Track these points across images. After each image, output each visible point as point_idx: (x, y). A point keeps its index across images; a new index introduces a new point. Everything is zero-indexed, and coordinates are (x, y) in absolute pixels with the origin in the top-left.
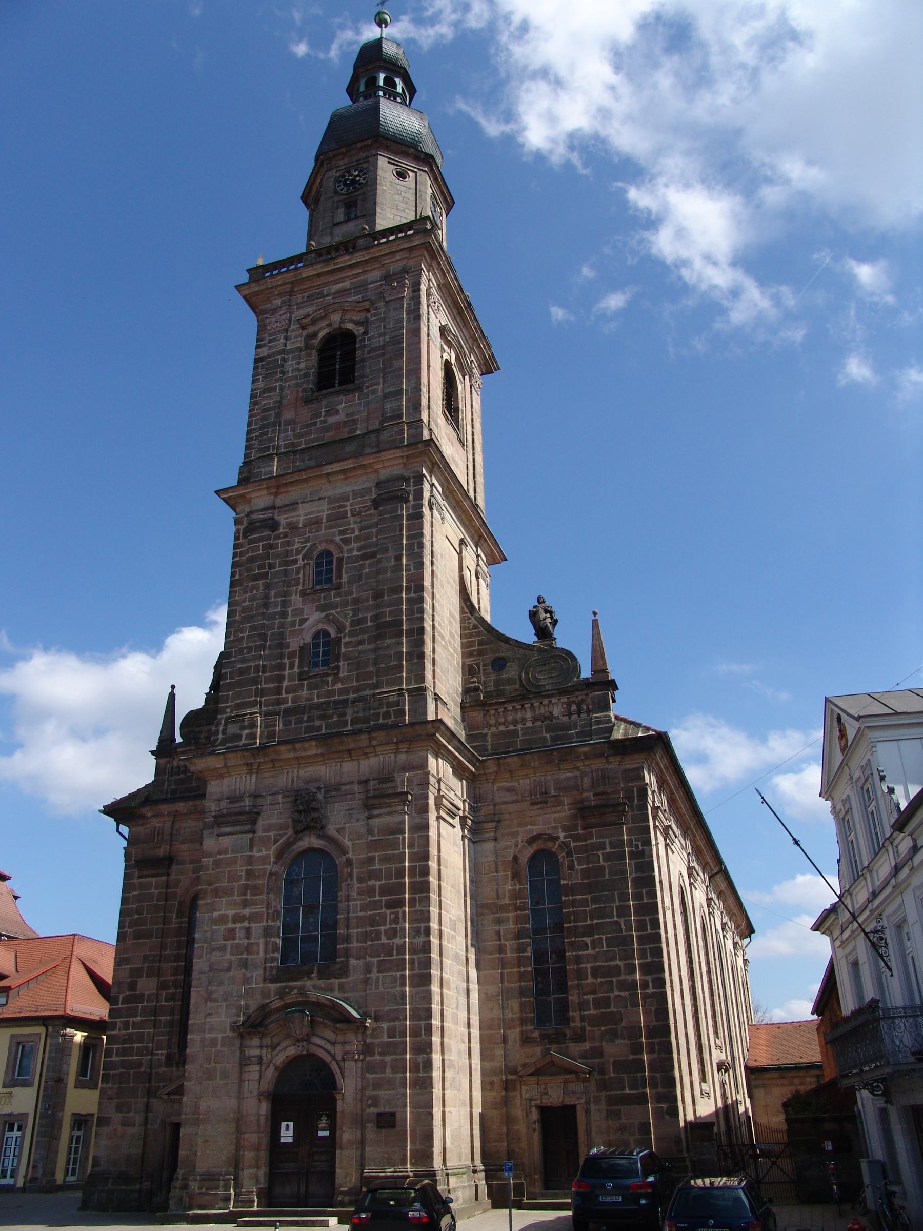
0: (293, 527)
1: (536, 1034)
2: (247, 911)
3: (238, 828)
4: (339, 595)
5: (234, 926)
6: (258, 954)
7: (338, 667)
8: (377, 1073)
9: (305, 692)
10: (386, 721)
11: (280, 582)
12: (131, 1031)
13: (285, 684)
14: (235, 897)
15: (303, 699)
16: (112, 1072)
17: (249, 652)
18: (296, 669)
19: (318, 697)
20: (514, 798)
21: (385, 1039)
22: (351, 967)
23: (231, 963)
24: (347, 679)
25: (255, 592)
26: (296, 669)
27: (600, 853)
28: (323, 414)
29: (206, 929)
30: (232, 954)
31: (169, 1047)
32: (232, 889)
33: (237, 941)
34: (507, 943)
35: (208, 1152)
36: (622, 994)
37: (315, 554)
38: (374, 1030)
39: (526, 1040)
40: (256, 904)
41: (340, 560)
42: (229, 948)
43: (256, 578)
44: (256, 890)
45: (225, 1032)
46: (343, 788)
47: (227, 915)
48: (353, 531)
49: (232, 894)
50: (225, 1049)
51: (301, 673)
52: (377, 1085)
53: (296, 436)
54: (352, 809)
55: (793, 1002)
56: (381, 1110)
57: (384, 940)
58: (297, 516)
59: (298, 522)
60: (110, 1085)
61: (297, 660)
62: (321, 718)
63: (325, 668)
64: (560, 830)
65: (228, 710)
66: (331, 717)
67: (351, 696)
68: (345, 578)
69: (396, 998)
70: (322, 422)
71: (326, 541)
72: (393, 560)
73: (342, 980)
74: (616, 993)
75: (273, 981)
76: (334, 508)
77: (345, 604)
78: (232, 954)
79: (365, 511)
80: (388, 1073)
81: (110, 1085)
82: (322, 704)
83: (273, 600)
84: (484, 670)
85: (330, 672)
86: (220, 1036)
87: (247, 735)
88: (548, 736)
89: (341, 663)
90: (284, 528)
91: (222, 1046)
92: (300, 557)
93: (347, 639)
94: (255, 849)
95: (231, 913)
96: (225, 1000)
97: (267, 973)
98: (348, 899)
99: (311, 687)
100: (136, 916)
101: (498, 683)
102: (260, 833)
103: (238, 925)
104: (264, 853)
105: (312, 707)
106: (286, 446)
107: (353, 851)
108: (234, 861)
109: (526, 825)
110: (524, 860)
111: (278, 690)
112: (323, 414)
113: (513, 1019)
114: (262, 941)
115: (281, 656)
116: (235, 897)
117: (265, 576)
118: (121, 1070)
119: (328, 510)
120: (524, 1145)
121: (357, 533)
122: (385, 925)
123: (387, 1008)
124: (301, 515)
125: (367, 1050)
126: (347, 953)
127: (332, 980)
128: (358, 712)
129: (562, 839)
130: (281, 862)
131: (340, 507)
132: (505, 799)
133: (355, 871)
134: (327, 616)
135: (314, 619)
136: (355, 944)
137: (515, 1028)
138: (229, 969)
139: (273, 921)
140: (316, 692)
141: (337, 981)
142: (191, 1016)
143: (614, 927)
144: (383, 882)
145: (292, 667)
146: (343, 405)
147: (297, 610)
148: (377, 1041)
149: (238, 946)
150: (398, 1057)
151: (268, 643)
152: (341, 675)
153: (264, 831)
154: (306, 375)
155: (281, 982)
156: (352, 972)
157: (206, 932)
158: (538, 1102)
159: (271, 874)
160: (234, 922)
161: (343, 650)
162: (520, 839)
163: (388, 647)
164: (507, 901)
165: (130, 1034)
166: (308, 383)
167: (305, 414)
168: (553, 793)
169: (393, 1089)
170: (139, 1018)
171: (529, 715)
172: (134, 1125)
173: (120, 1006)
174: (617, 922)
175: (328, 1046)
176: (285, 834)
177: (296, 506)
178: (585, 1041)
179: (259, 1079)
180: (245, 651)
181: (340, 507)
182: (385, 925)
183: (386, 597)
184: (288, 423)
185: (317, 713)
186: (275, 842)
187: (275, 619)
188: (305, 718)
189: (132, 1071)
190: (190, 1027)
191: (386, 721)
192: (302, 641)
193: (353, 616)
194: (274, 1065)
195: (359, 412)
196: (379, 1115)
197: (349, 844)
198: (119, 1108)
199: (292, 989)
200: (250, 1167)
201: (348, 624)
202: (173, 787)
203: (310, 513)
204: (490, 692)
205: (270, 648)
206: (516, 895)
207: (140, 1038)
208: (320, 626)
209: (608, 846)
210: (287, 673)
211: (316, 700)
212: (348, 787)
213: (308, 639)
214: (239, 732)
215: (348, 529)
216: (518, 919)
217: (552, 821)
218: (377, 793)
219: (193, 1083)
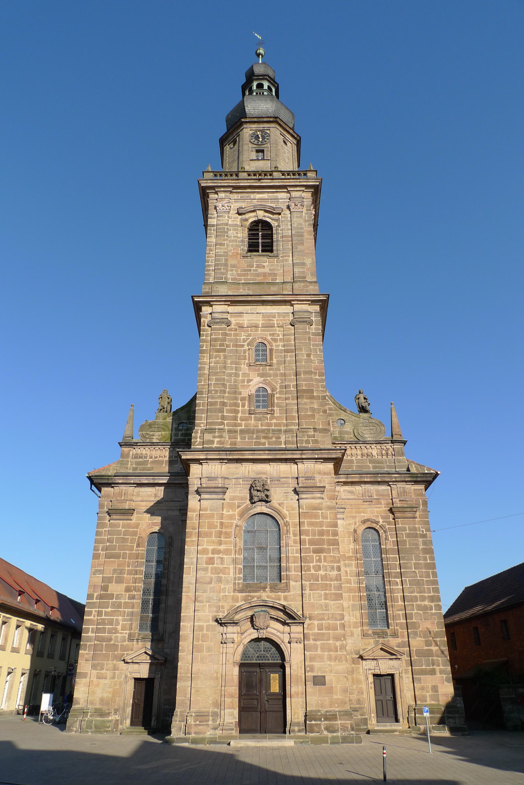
0: (241, 327)
1: (370, 632)
2: (222, 547)
3: (214, 496)
4: (272, 369)
5: (213, 556)
6: (229, 574)
8: (312, 651)
9: (253, 421)
10: (307, 445)
11: (233, 356)
12: (103, 617)
13: (240, 415)
14: (213, 538)
15: (252, 426)
16: (88, 643)
17: (215, 393)
18: (246, 407)
19: (262, 425)
21: (316, 631)
22: (291, 586)
23: (211, 579)
24: (277, 418)
25: (218, 359)
26: (246, 407)
27: (404, 533)
28: (255, 266)
30: (212, 573)
31: (131, 629)
32: (211, 533)
33: (215, 565)
34: (352, 578)
35: (198, 698)
36: (419, 612)
39: (364, 635)
40: (227, 544)
41: (271, 350)
42: (210, 569)
43: (218, 351)
45: (208, 621)
46: (282, 480)
47: (208, 549)
48: (278, 335)
49: (211, 536)
50: (209, 633)
51: (250, 410)
52: (312, 659)
53: (239, 275)
55: (59, 621)
56: (316, 674)
57: (313, 572)
58: (243, 320)
59: (244, 324)
60: (87, 652)
61: (247, 402)
62: (265, 438)
63: (265, 409)
64: (380, 518)
65: (202, 425)
66: (271, 438)
67: (283, 428)
68: (275, 361)
70: (254, 270)
71: (262, 338)
72: (305, 356)
73: (286, 594)
74: (416, 611)
75: (241, 591)
76: (267, 320)
77: (276, 375)
78: (212, 573)
79: (285, 326)
80: (319, 652)
81: (87, 652)
82: (264, 430)
83: (229, 365)
84: (333, 424)
85: (268, 412)
86: (205, 624)
88: (371, 465)
89: (275, 408)
90: (234, 325)
91: (207, 631)
92: (246, 343)
93: (278, 395)
94: (225, 510)
95: (210, 548)
96: (209, 602)
98: (287, 545)
99: (256, 419)
100: (108, 544)
101: (340, 433)
102: (228, 500)
105: (258, 431)
106: (232, 279)
107: (289, 517)
108: (212, 516)
109: (360, 513)
110: (360, 531)
111: (235, 418)
112: (255, 266)
113: (356, 623)
114: (232, 567)
115: (236, 399)
116: (213, 538)
117: (224, 351)
118: (96, 642)
119: (262, 320)
120: (365, 696)
121: (281, 337)
122: (313, 562)
123: (316, 612)
124: (245, 320)
125: (305, 636)
126: (288, 578)
127: (280, 593)
128: (288, 438)
129: (381, 523)
133: (291, 529)
134: (264, 380)
135: (256, 382)
136: (293, 573)
137: (357, 627)
138: (210, 583)
139: (239, 555)
140: (260, 422)
141: (283, 594)
142: (182, 611)
143: (413, 575)
144: (310, 537)
145: (243, 406)
146: (267, 263)
147: (245, 373)
149: (216, 568)
150: (326, 642)
151: (227, 390)
152: (275, 415)
154: (242, 241)
155: (246, 592)
156: (292, 589)
158: (373, 671)
159: (237, 526)
160: (213, 553)
161: (276, 401)
162: (357, 520)
163: (305, 404)
165: (104, 620)
166: (244, 246)
167: (244, 263)
168: (375, 497)
169: (322, 662)
170: (109, 609)
171: (359, 452)
172: (106, 678)
173: (95, 600)
174: (415, 571)
175: (278, 634)
177: (242, 314)
178: (398, 637)
179: (235, 653)
180: (213, 392)
182: (313, 562)
183: (302, 376)
184: (233, 266)
185: (262, 435)
186: (239, 507)
188: (255, 437)
189: (104, 643)
190: (182, 618)
191: (307, 445)
192: (250, 392)
193: (282, 383)
194: (243, 644)
196: (314, 677)
197: (287, 513)
198: (94, 667)
199: (253, 597)
200: (229, 708)
201: (278, 387)
202: (134, 466)
204: (336, 437)
205: (229, 393)
206: (356, 552)
207: (111, 622)
209: (407, 529)
210: (240, 409)
211: (260, 427)
212: (285, 479)
213: (253, 392)
214: (212, 439)
215: (276, 334)
216: (357, 566)
217: (378, 512)
219: (185, 654)
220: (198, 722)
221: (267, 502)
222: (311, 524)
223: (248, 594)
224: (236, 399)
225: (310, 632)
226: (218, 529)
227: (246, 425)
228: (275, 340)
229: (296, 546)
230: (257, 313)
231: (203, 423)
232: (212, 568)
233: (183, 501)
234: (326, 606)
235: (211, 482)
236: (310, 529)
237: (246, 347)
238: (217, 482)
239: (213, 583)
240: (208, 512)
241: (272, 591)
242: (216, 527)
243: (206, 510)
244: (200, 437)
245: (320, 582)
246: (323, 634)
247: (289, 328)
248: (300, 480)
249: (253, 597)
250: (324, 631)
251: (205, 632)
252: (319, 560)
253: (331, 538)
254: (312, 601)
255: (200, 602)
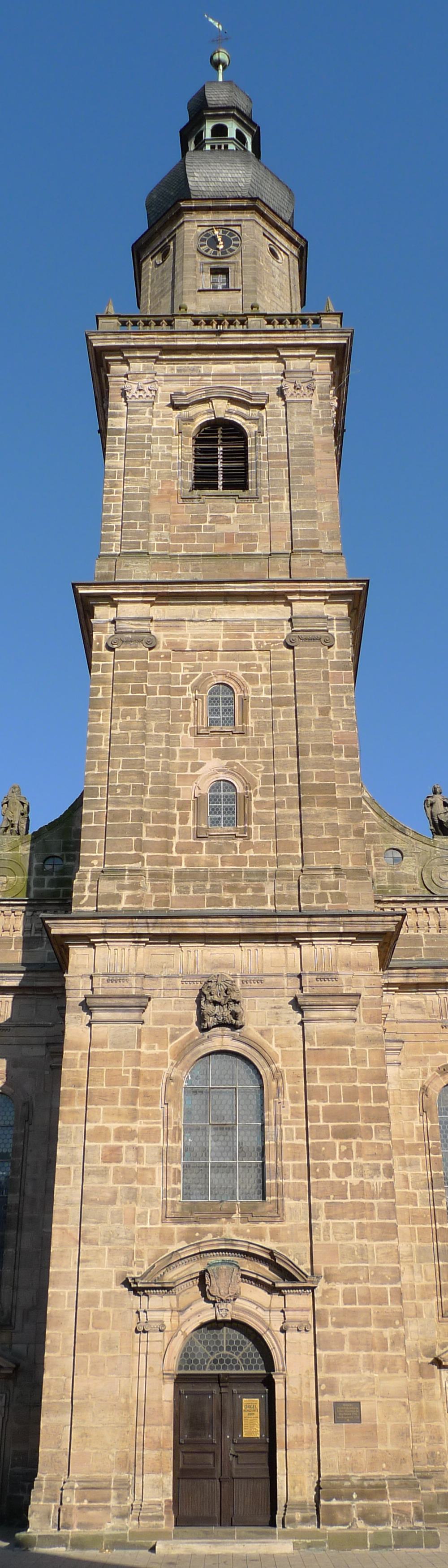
0: (179, 650)
3: (120, 1015)
4: (245, 742)
5: (118, 1144)
6: (153, 1183)
7: (247, 830)
8: (331, 1349)
9: (204, 854)
11: (162, 712)
13: (176, 840)
15: (202, 863)
17: (123, 793)
18: (190, 824)
19: (223, 863)
20: (420, 1017)
21: (341, 1305)
22: (286, 1209)
23: (115, 1193)
24: (256, 847)
25: (128, 719)
29: (73, 1145)
30: (116, 1181)
32: (114, 1095)
33: (123, 1164)
35: (87, 1450)
37: (209, 687)
38: (325, 1292)
40: (148, 1118)
41: (244, 700)
42: (111, 1173)
43: (130, 702)
44: (150, 1099)
46: (267, 980)
47: (107, 1129)
48: (259, 668)
50: (111, 1310)
51: (197, 830)
52: (332, 1366)
53: (174, 538)
54: (280, 1008)
56: (339, 1399)
57: (333, 1177)
58: (183, 636)
59: (185, 643)
61: (191, 812)
62: (230, 889)
65: (95, 862)
66: (244, 890)
67: (269, 868)
68: (251, 723)
69: (353, 1253)
71: (225, 674)
72: (317, 712)
75: (178, 1220)
76: (234, 636)
77: (254, 754)
78: (116, 1181)
82: (229, 873)
84: (376, 860)
86: (101, 1291)
87: (128, 897)
89: (252, 826)
90: (164, 647)
91: (105, 1305)
92: (189, 686)
93: (258, 798)
94: (144, 1045)
95: (113, 1126)
97: (169, 1210)
98: (278, 1121)
99: (211, 849)
102: (149, 1024)
103: (125, 1144)
104: (157, 1051)
105: (215, 875)
106: (159, 547)
107: (283, 1060)
108: (116, 1058)
111: (167, 847)
112: (209, 519)
114: (158, 1167)
115: (168, 805)
116: (119, 1106)
117: (142, 701)
121: (265, 671)
122: (334, 1158)
123: (341, 1265)
124: (188, 636)
127: (262, 1225)
128: (281, 889)
130: (181, 1066)
131: (241, 636)
132: (410, 1017)
133: (287, 1085)
134: (228, 765)
135: (212, 768)
136: (291, 1180)
138: (112, 1201)
140: (220, 856)
141: (268, 1226)
144: (328, 1103)
145: (184, 820)
146: (235, 513)
147: (188, 750)
148: (329, 1307)
149: (124, 1171)
150: (361, 1329)
151: (149, 786)
152: (252, 840)
153: (156, 1022)
154: (182, 466)
155: (189, 1222)
156: (288, 1216)
157: (73, 1148)
159: (170, 1079)
160: (118, 1138)
161: (254, 810)
162: (429, 1067)
163: (317, 816)
164: (415, 1141)
167: (185, 512)
169: (354, 1371)
175: (259, 1312)
176: (186, 1029)
177: (182, 623)
179: (165, 1353)
180: (119, 791)
181: (241, 636)
182: (334, 1158)
183: (310, 756)
184: (162, 519)
186: (174, 1037)
187: (159, 757)
188: (208, 887)
190: (51, 1278)
194: (184, 1333)
195: (258, 527)
196: (336, 1404)
197: (278, 1051)
199: (204, 1233)
200: (153, 1472)
201: (259, 779)
203: (200, 636)
204: (384, 887)
208: (222, 776)
210: (177, 826)
211: (220, 867)
212: (273, 979)
213: (205, 790)
214: (116, 892)
215: (253, 665)
218: (316, 991)
219: (58, 1354)
220: (86, 1503)
221: (234, 1027)
222: (330, 1075)
223: (193, 1226)
224: (168, 805)
225: (329, 1307)
226: (130, 1086)
227: (189, 862)
228: (253, 679)
229: (297, 1123)
230: (214, 621)
231: (96, 858)
232: (116, 1171)
233: (53, 1026)
234: (363, 1251)
235: (113, 985)
236: (328, 1085)
237: (190, 695)
238: (126, 984)
239: (118, 1202)
240: (108, 1050)
241: (244, 1220)
242: (125, 1081)
243: (103, 1044)
244: (91, 887)
245: (349, 1200)
246: (355, 1312)
247: (282, 653)
248: (306, 979)
249: (204, 1233)
250: (358, 1306)
251: (101, 1307)
252: (348, 1154)
253: (373, 1105)
254: (332, 1240)
255: (91, 1242)
